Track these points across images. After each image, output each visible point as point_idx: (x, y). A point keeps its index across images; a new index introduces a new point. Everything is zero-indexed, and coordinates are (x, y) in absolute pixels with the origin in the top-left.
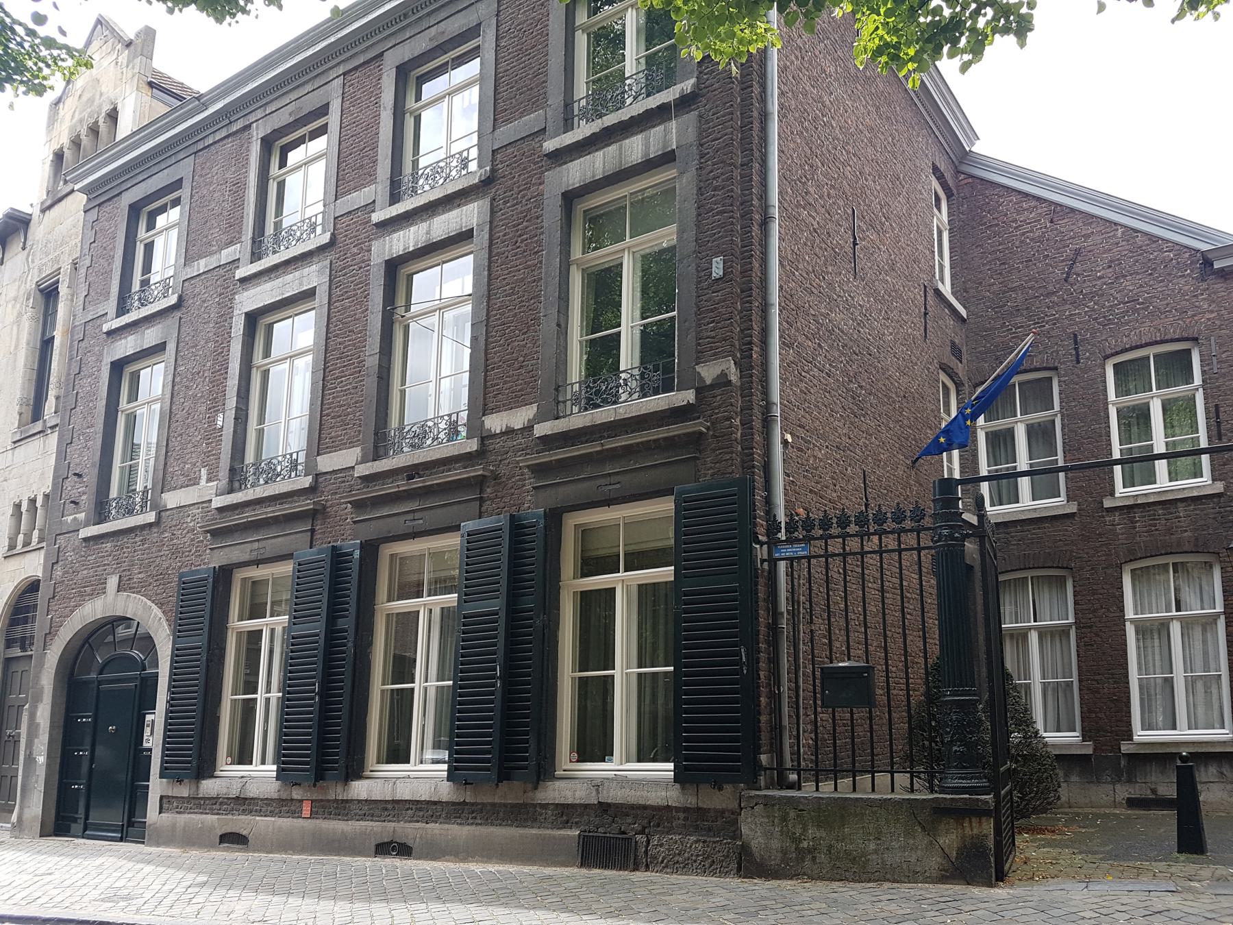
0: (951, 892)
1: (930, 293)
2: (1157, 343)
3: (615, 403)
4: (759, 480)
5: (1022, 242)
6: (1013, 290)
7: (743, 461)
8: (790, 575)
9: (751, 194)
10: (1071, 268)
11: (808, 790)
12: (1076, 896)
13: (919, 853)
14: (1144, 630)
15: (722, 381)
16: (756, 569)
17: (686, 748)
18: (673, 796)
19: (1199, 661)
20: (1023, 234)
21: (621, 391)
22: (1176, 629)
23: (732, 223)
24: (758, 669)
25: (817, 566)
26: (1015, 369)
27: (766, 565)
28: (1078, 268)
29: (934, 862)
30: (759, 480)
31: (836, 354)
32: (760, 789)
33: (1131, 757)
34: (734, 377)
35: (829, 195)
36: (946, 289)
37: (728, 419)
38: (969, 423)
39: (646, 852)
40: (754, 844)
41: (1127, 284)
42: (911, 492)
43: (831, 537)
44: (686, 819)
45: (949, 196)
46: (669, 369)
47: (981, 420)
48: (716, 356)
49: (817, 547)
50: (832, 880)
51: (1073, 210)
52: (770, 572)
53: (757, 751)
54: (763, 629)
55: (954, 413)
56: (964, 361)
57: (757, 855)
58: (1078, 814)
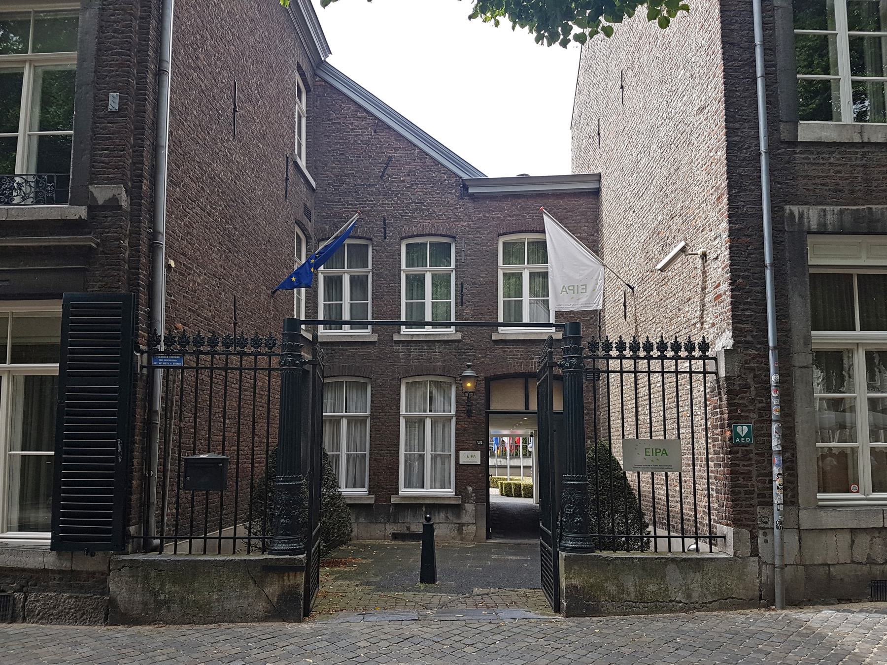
0: (270, 630)
1: (291, 164)
2: (431, 235)
3: (7, 204)
4: (143, 297)
5: (355, 141)
6: (348, 175)
7: (129, 279)
8: (166, 378)
9: (148, 45)
10: (385, 169)
11: (168, 554)
12: (356, 626)
13: (250, 600)
14: (409, 421)
15: (113, 204)
16: (136, 374)
17: (63, 522)
18: (50, 561)
19: (439, 447)
20: (356, 135)
21: (15, 194)
22: (428, 423)
23: (129, 66)
24: (132, 458)
25: (189, 375)
26: (347, 235)
27: (145, 371)
28: (390, 170)
29: (260, 607)
30: (143, 297)
31: (216, 198)
32: (127, 554)
33: (396, 505)
34: (125, 203)
35: (215, 64)
36: (302, 163)
37: (118, 239)
38: (312, 270)
39: (23, 607)
40: (119, 598)
41: (418, 190)
42: (270, 315)
43: (202, 353)
44: (61, 579)
45: (308, 91)
46: (63, 182)
47: (321, 268)
48: (109, 181)
49: (191, 360)
50: (182, 623)
51: (389, 127)
52: (148, 376)
53: (127, 523)
54: (139, 424)
55: (304, 261)
56: (313, 220)
57: (121, 607)
58: (362, 546)
